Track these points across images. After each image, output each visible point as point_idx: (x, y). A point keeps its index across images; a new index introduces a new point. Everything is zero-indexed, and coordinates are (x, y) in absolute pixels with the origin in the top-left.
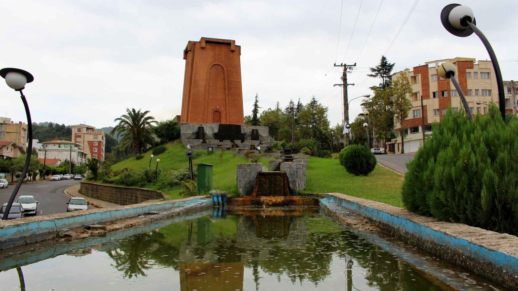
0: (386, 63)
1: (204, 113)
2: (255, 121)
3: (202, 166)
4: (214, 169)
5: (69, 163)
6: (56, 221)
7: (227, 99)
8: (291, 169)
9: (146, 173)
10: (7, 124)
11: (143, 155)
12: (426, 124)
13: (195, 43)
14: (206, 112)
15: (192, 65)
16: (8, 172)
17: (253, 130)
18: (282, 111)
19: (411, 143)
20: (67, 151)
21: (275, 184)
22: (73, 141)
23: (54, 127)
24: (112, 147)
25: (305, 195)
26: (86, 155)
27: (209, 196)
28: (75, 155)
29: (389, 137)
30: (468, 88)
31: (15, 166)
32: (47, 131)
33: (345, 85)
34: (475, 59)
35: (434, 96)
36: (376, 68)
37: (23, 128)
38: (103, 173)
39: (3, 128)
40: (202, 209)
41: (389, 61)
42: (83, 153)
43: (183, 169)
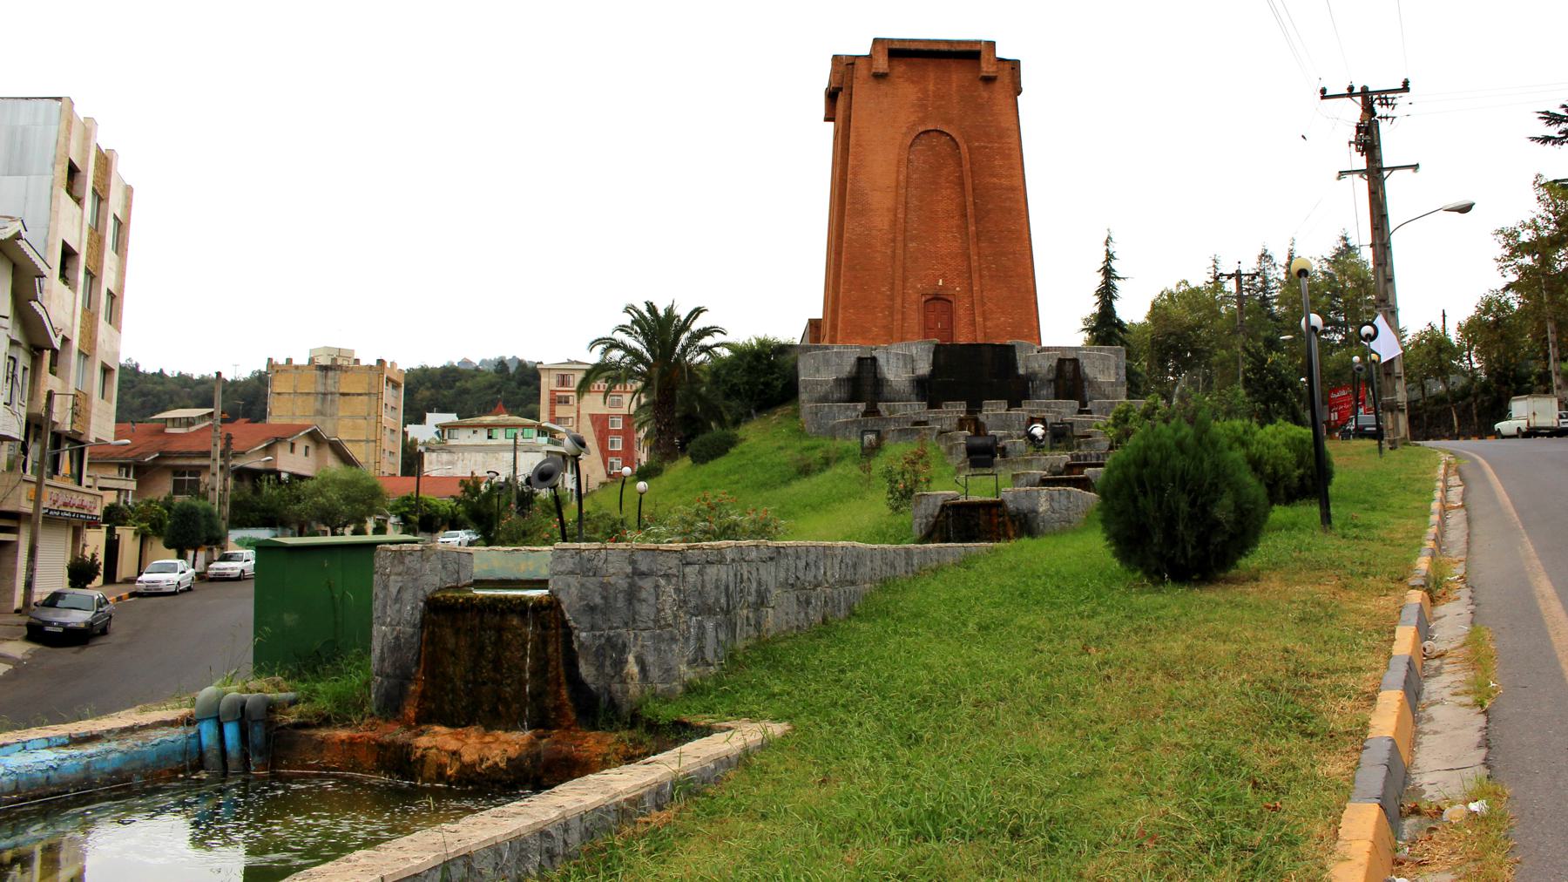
7: (973, 251)
8: (592, 582)
10: (340, 367)
14: (899, 301)
23: (512, 369)
32: (491, 386)
33: (1375, 174)
37: (389, 379)
39: (330, 382)
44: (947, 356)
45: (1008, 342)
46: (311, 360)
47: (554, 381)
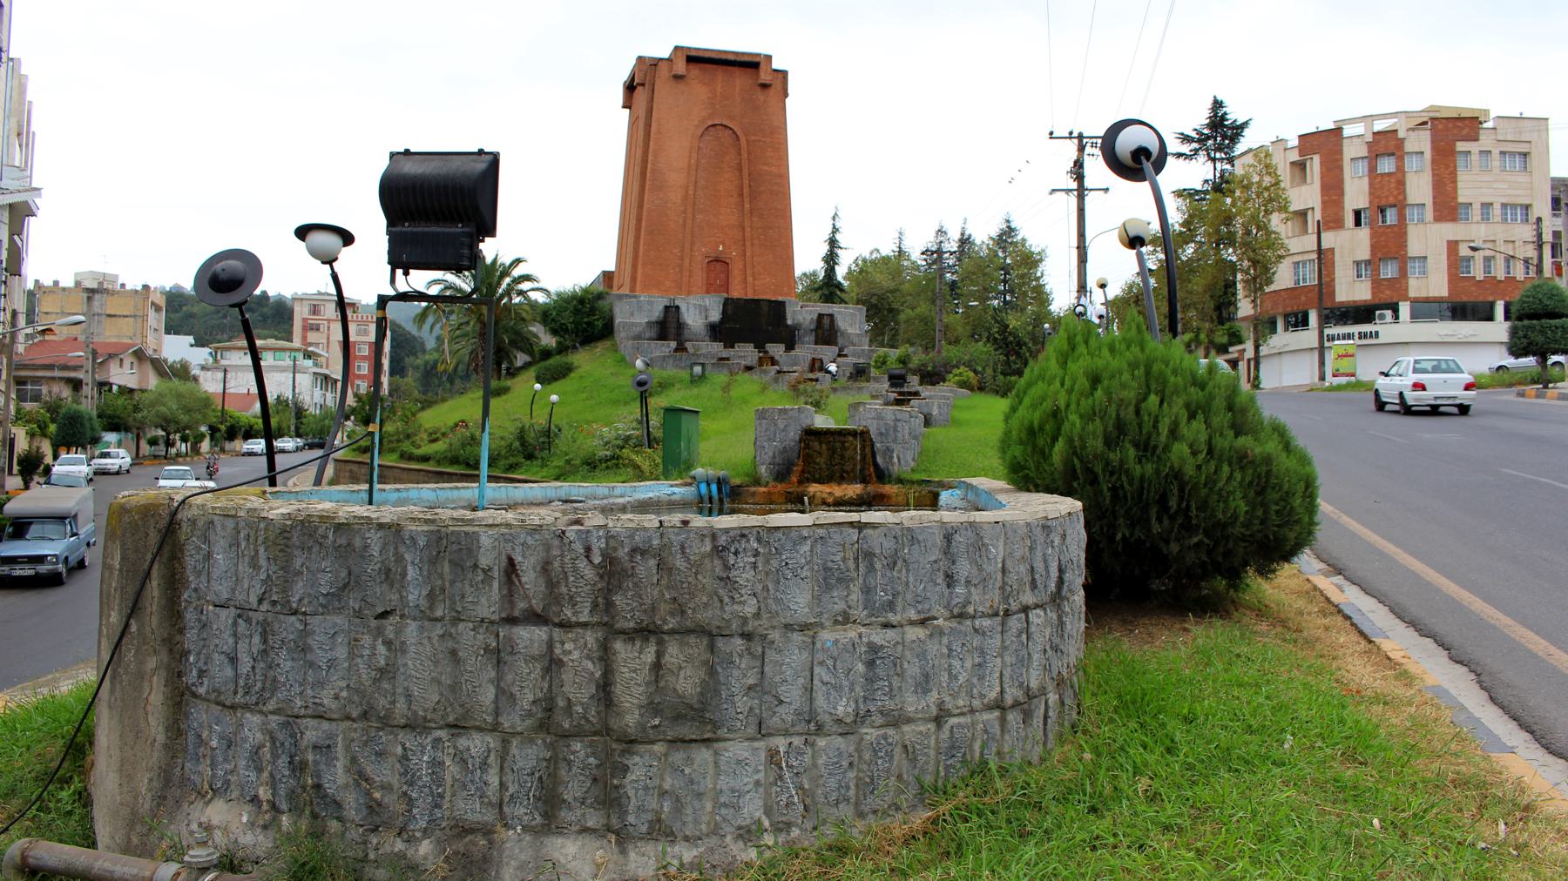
0: (1223, 118)
2: (828, 288)
3: (673, 412)
4: (704, 423)
7: (747, 224)
9: (521, 436)
10: (107, 291)
11: (509, 383)
12: (1329, 305)
13: (655, 63)
14: (687, 261)
15: (648, 125)
16: (127, 429)
17: (821, 316)
19: (1285, 358)
20: (283, 370)
21: (842, 457)
22: (297, 343)
24: (409, 360)
28: (304, 381)
30: (1461, 200)
33: (1081, 192)
34: (1486, 112)
35: (1358, 223)
36: (1194, 134)
38: (398, 432)
40: (673, 505)
41: (1235, 114)
42: (326, 377)
43: (624, 420)
44: (734, 309)
46: (78, 284)
47: (306, 310)
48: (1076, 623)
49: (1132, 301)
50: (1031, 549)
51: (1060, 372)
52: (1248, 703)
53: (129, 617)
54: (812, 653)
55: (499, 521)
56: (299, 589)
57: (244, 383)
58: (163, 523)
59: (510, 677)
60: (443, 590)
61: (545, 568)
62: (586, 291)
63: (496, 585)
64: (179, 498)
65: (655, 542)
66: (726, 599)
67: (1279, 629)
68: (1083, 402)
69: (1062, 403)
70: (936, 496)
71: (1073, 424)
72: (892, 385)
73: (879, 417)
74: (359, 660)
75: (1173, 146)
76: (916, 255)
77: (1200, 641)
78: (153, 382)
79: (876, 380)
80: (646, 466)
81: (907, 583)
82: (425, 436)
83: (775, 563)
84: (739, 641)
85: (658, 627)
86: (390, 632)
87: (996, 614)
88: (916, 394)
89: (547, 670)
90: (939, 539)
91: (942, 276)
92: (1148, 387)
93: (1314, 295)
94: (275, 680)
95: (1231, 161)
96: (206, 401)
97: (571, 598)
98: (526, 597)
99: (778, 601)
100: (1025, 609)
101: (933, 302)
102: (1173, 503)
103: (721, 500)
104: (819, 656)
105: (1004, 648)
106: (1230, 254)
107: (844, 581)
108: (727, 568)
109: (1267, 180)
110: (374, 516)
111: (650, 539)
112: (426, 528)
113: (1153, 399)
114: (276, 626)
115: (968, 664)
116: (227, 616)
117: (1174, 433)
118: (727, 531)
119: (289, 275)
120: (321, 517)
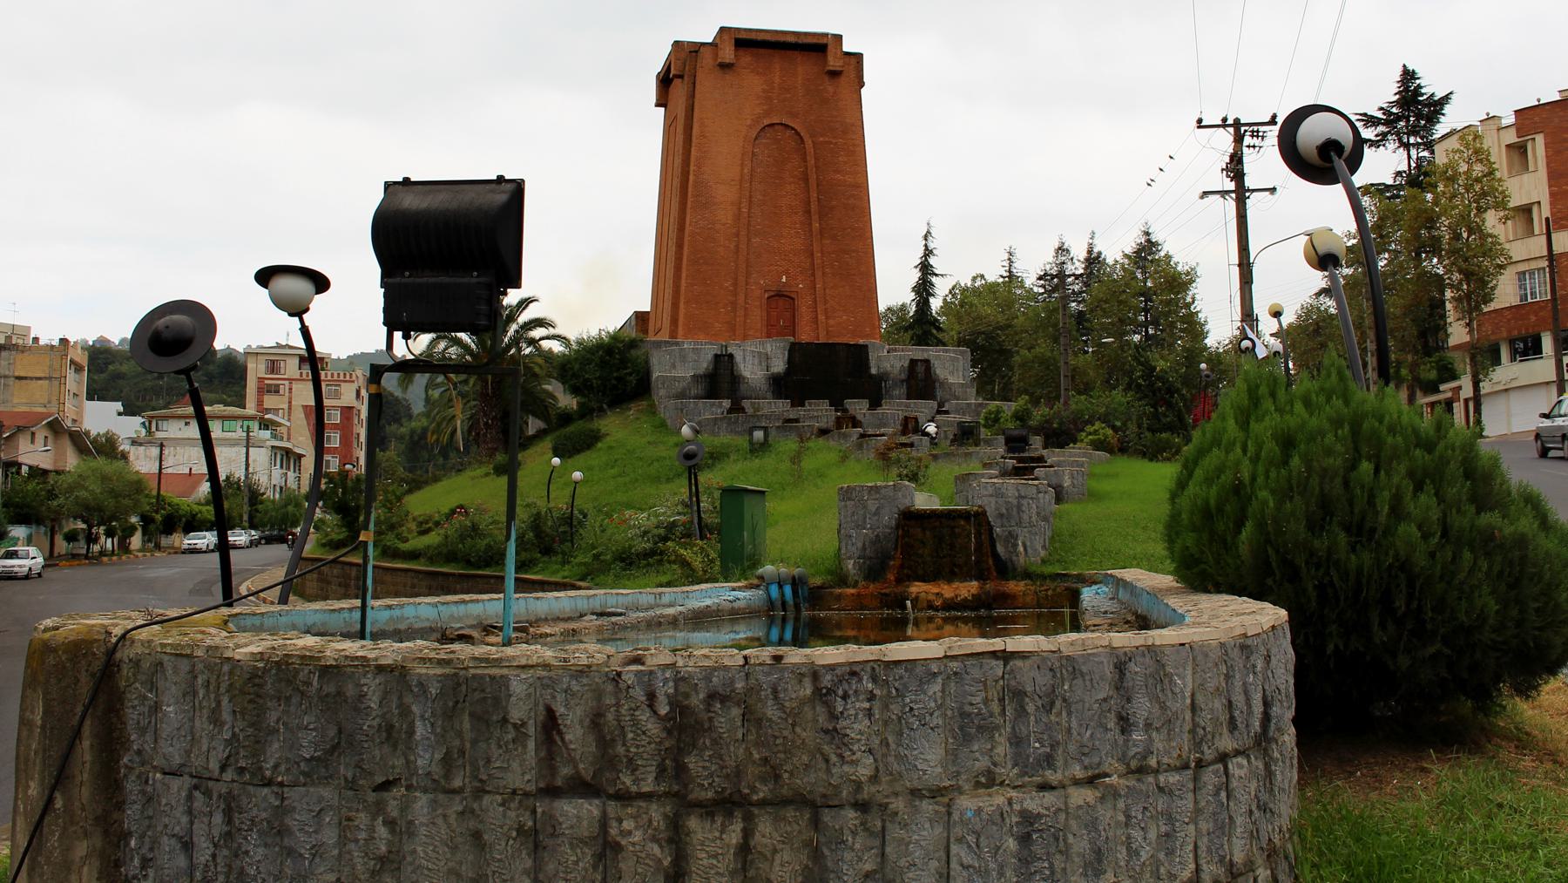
0: (1417, 91)
1: (734, 304)
2: (920, 325)
3: (733, 495)
4: (771, 505)
5: (239, 488)
6: (441, 608)
7: (816, 247)
8: (1000, 501)
14: (741, 297)
17: (913, 362)
18: (1028, 283)
19: (1513, 396)
20: (233, 443)
22: (251, 409)
24: (392, 429)
25: (1043, 577)
26: (300, 456)
27: (755, 581)
28: (260, 457)
29: (1433, 375)
31: (61, 500)
36: (1379, 115)
37: (72, 362)
41: (1432, 86)
42: (288, 452)
45: (861, 342)
47: (262, 367)
48: (1287, 774)
49: (1309, 335)
50: (1228, 677)
51: (1241, 435)
52: (1524, 872)
53: (53, 789)
54: (948, 826)
55: (534, 660)
56: (274, 751)
57: (187, 459)
58: (97, 666)
59: (551, 867)
60: (462, 752)
61: (596, 721)
62: (615, 337)
63: (531, 745)
64: (117, 631)
65: (739, 685)
66: (834, 758)
67: (1549, 766)
68: (1273, 474)
69: (1246, 476)
70: (1075, 597)
71: (1265, 503)
72: (1010, 450)
73: (998, 493)
74: (352, 846)
75: (1368, 133)
76: (1030, 280)
77: (1447, 787)
78: (72, 461)
79: (988, 442)
80: (697, 562)
81: (1069, 730)
82: (413, 526)
83: (895, 709)
84: (851, 814)
85: (745, 797)
86: (393, 809)
87: (1186, 767)
88: (1041, 459)
89: (600, 857)
90: (1108, 670)
91: (1065, 307)
92: (1357, 449)
93: (1546, 314)
94: (242, 872)
95: (1429, 146)
96: (138, 485)
97: (630, 760)
98: (572, 761)
99: (901, 758)
100: (1223, 758)
101: (1056, 340)
102: (1400, 603)
103: (797, 607)
104: (958, 831)
105: (1198, 811)
106: (1435, 265)
107: (988, 730)
108: (833, 717)
109: (1478, 169)
110: (371, 655)
111: (732, 681)
112: (439, 671)
113: (1366, 467)
114: (245, 800)
115: (1152, 835)
116: (180, 786)
117: (1397, 511)
118: (831, 668)
119: (247, 325)
120: (303, 657)
